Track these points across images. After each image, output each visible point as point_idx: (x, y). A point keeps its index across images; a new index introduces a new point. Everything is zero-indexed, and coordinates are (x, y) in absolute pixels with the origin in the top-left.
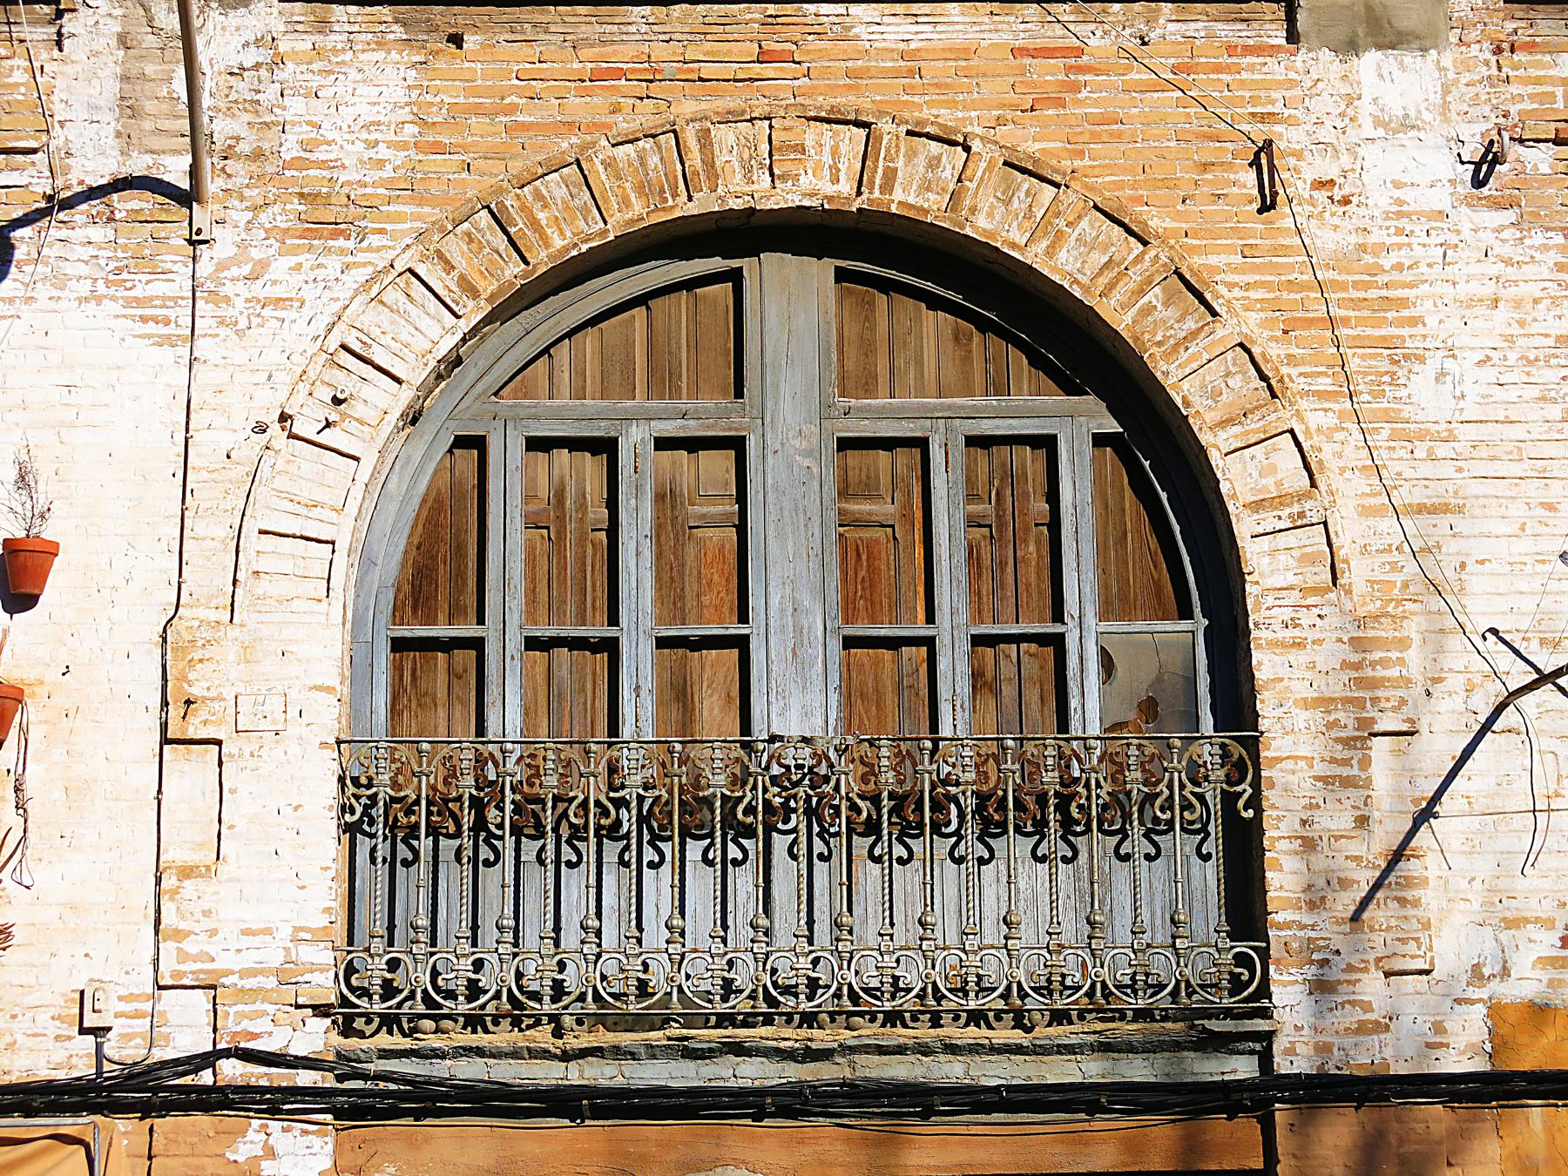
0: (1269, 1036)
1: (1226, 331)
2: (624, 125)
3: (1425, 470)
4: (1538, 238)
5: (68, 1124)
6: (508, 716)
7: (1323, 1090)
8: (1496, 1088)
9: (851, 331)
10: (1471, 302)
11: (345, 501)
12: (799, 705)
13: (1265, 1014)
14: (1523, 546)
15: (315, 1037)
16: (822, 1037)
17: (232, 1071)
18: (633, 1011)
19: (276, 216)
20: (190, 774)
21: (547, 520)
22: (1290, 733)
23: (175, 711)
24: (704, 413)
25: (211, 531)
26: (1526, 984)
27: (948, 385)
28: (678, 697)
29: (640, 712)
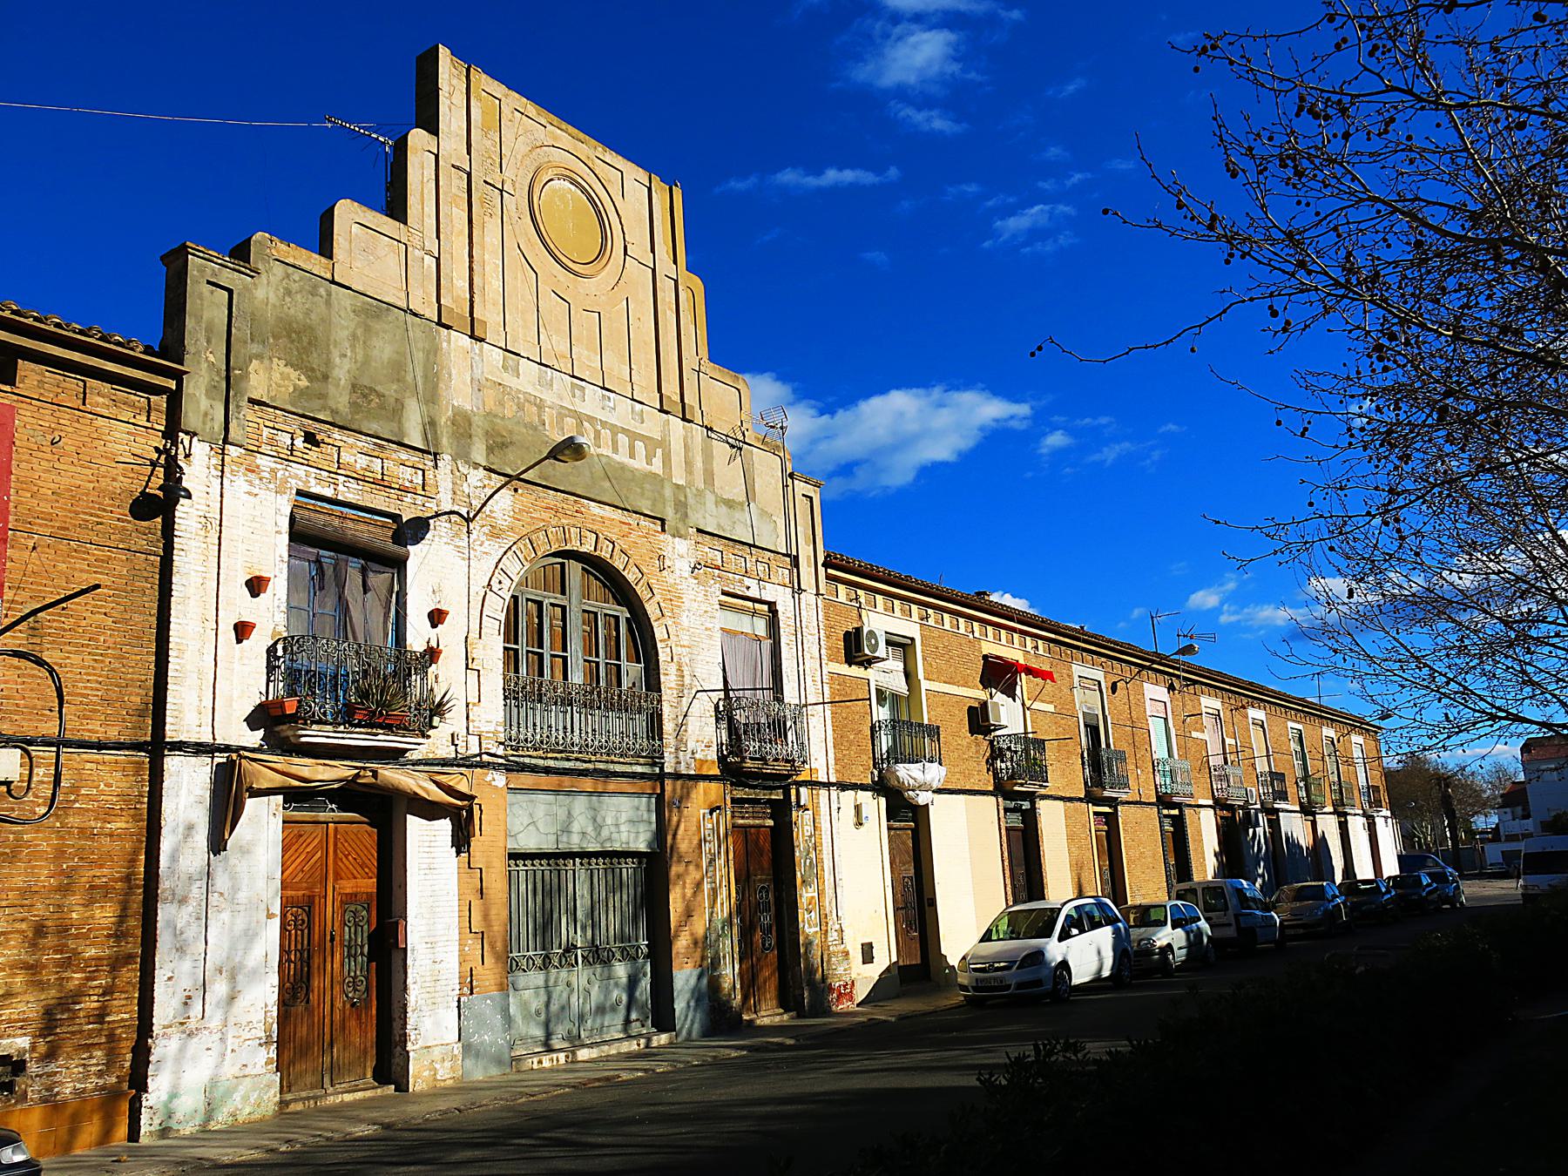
5: (463, 770)
11: (497, 608)
12: (577, 678)
17: (485, 758)
25: (475, 613)
29: (547, 671)
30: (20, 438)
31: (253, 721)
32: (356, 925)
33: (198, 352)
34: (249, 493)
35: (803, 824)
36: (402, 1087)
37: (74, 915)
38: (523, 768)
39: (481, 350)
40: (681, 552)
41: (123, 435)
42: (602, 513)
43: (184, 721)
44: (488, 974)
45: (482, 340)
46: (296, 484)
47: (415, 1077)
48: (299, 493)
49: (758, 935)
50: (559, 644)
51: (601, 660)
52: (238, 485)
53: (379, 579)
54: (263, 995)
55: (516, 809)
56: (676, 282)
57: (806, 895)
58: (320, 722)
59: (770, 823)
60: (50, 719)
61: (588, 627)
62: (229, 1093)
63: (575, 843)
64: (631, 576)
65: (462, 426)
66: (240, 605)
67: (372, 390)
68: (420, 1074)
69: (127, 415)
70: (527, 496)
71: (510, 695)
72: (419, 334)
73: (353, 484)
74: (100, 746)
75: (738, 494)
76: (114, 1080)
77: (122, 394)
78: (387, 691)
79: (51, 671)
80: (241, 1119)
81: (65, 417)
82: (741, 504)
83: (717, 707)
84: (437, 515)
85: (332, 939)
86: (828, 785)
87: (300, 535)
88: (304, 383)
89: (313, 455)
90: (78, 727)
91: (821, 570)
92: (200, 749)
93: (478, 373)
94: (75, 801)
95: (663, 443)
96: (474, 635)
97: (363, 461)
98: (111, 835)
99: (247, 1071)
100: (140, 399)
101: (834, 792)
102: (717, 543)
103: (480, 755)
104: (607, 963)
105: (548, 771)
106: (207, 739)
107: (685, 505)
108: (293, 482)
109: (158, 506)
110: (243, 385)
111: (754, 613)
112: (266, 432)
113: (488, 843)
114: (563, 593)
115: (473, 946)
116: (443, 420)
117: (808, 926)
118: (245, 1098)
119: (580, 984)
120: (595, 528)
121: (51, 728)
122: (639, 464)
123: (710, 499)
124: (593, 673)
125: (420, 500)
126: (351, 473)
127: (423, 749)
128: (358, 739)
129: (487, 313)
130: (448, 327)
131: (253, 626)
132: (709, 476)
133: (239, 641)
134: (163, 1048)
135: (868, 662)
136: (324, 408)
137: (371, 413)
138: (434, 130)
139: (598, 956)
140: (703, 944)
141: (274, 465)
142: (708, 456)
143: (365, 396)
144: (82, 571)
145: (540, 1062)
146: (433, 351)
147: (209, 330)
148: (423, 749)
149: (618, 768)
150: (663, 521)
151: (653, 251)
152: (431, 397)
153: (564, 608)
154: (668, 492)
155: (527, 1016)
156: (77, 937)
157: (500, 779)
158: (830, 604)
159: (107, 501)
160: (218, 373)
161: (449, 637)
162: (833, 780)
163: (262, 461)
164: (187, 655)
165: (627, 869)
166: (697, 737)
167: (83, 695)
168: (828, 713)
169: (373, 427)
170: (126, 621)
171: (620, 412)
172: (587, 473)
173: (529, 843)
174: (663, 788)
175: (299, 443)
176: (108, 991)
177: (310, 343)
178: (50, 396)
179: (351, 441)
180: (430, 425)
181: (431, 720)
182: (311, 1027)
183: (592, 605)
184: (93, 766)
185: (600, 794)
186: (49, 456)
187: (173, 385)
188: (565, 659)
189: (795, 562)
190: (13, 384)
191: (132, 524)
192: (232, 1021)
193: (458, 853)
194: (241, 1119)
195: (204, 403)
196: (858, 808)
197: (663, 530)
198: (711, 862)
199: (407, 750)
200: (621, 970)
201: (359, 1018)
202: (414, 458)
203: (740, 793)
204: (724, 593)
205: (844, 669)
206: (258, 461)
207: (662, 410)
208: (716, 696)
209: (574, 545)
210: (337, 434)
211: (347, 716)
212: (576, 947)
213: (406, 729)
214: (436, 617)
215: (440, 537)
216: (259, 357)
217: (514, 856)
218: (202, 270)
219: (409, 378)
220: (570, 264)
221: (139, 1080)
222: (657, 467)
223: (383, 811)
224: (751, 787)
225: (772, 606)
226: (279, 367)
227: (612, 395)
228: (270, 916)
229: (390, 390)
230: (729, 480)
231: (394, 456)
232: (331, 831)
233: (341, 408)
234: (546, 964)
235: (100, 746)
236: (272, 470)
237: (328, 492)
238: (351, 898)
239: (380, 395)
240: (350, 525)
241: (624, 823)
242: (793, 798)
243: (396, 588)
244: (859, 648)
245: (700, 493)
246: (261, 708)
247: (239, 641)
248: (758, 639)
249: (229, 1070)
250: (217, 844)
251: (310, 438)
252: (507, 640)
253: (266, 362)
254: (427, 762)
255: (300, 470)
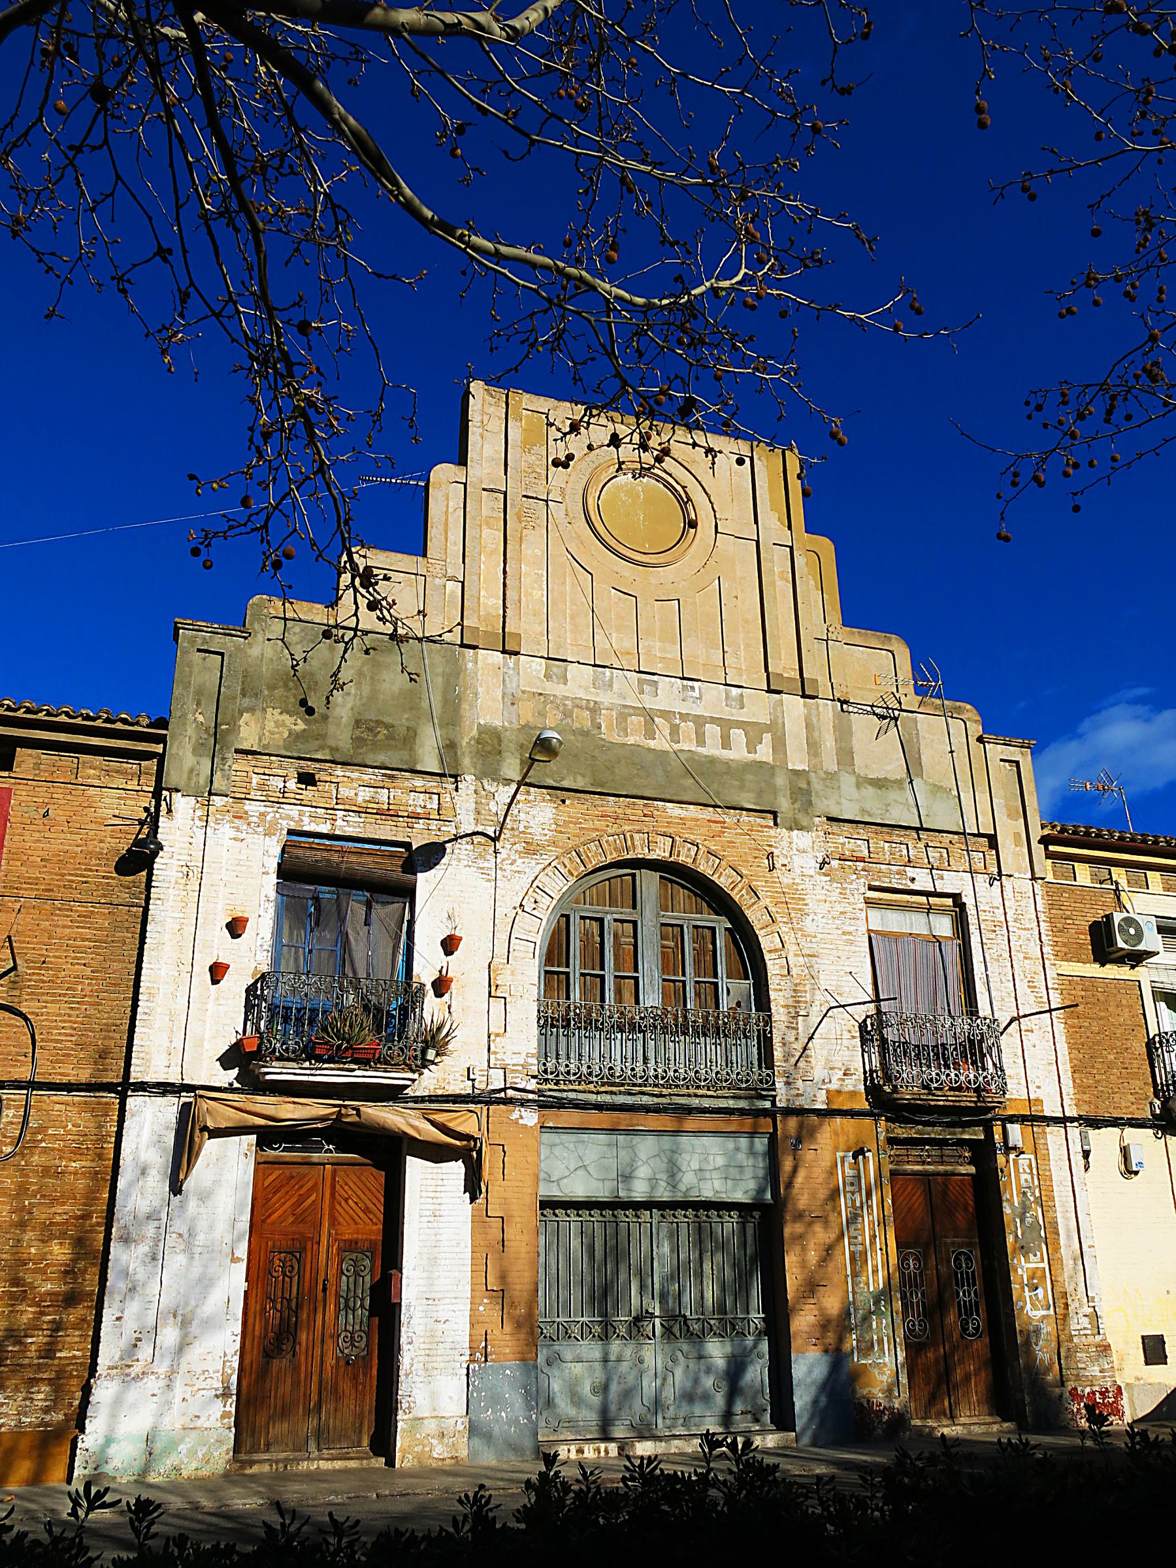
0: (775, 1097)
1: (762, 903)
2: (610, 831)
3: (810, 945)
4: (835, 885)
5: (472, 1106)
6: (576, 994)
7: (788, 1112)
8: (830, 1113)
9: (816, 734)
10: (819, 901)
11: (535, 931)
12: (651, 999)
13: (774, 1090)
14: (832, 967)
15: (532, 1085)
16: (665, 1092)
17: (510, 1093)
18: (609, 1080)
19: (518, 847)
20: (497, 1006)
21: (586, 937)
22: (779, 1013)
23: (493, 988)
24: (627, 913)
25: (502, 937)
26: (834, 1086)
27: (694, 917)
28: (619, 991)
29: (610, 996)
30: (14, 814)
31: (226, 1061)
32: (356, 1274)
33: (184, 715)
34: (235, 839)
35: (1017, 1175)
36: (390, 1462)
37: (33, 1250)
38: (560, 1104)
39: (517, 664)
40: (800, 849)
41: (112, 799)
42: (683, 813)
43: (150, 1064)
44: (505, 1341)
45: (517, 653)
46: (286, 825)
47: (403, 1451)
48: (291, 832)
49: (952, 1317)
50: (630, 960)
51: (687, 978)
52: (224, 832)
53: (385, 912)
54: (220, 1347)
55: (557, 1151)
56: (791, 548)
57: (1023, 1267)
58: (281, 1059)
59: (972, 1169)
60: (23, 1064)
61: (665, 947)
62: (172, 1445)
63: (639, 1191)
64: (723, 881)
65: (490, 745)
66: (221, 947)
67: (379, 723)
68: (409, 1446)
69: (120, 782)
70: (574, 807)
71: (547, 1023)
72: (438, 659)
73: (353, 818)
74: (69, 1087)
75: (895, 767)
76: (61, 1417)
77: (114, 763)
78: (395, 1024)
79: (26, 1019)
80: (185, 1473)
81: (59, 792)
82: (899, 782)
83: (862, 1027)
84: (456, 838)
85: (324, 1290)
86: (1063, 1121)
87: (289, 872)
88: (301, 726)
89: (309, 793)
90: (48, 1071)
91: (1039, 850)
92: (165, 1089)
93: (511, 686)
94: (41, 1141)
95: (776, 730)
96: (500, 960)
97: (364, 794)
98: (75, 1174)
99: (199, 1423)
100: (132, 766)
101: (1074, 1131)
102: (863, 832)
103: (504, 1090)
104: (696, 1339)
105: (599, 1107)
106: (175, 1078)
107: (808, 792)
108: (284, 823)
109: (139, 859)
110: (231, 738)
111: (929, 910)
112: (255, 779)
113: (511, 1188)
114: (634, 907)
115: (489, 1311)
116: (466, 740)
117: (1032, 1308)
118: (192, 1453)
119: (652, 1363)
120: (671, 831)
121: (23, 1073)
122: (738, 752)
123: (847, 782)
124: (674, 992)
125: (434, 825)
126: (351, 808)
127: (427, 1082)
128: (330, 1075)
129: (526, 626)
130: (475, 647)
131: (227, 967)
132: (846, 756)
133: (215, 981)
134: (103, 1392)
135: (1137, 958)
136: (321, 748)
137: (380, 744)
138: (462, 461)
139: (679, 1328)
140: (836, 1329)
141: (263, 809)
142: (843, 733)
143: (370, 730)
144: (64, 927)
145: (580, 1451)
146: (455, 674)
147: (199, 693)
148: (427, 1082)
149: (706, 1103)
150: (775, 814)
151: (756, 522)
152: (452, 715)
153: (635, 923)
154: (781, 781)
155: (576, 1399)
156: (35, 1271)
157: (530, 1118)
158: (1055, 895)
159: (94, 862)
160: (207, 730)
161: (466, 968)
162: (1071, 1112)
163: (249, 806)
164: (159, 999)
165: (730, 1224)
166: (830, 1062)
167: (57, 1041)
168: (1059, 1028)
169: (381, 758)
170: (105, 970)
171: (710, 700)
172: (659, 772)
173: (578, 1189)
174: (774, 1125)
175: (292, 784)
176: (57, 1326)
177: (309, 688)
178: (45, 776)
179: (355, 775)
180: (450, 748)
181: (424, 1052)
182: (296, 1384)
183: (671, 917)
184: (63, 1107)
185: (677, 1133)
186: (41, 827)
187: (159, 748)
188: (636, 979)
189: (993, 841)
190: (10, 769)
191: (116, 879)
192: (183, 1368)
193: (473, 1199)
194: (185, 1473)
195: (189, 760)
196: (1125, 1152)
197: (776, 824)
198: (853, 1219)
199: (407, 1086)
200: (717, 1351)
201: (355, 1378)
202: (432, 784)
203: (901, 1132)
204: (871, 888)
205: (1094, 970)
206: (246, 808)
207: (769, 691)
208: (860, 1012)
209: (641, 852)
210: (339, 771)
211: (309, 1054)
212: (652, 1316)
213: (387, 1063)
214: (450, 945)
215: (457, 859)
216: (251, 710)
217: (547, 1205)
218: (192, 641)
219: (425, 704)
220: (638, 557)
221: (80, 1421)
222: (764, 752)
223: (387, 1153)
224: (925, 1124)
225: (956, 897)
226: (273, 716)
227: (696, 684)
228: (235, 1260)
229: (402, 720)
230: (878, 752)
231: (407, 784)
232: (328, 1174)
233: (341, 744)
234: (606, 1333)
235: (69, 1087)
236: (263, 814)
237: (324, 828)
238: (350, 1246)
239: (388, 726)
240: (353, 858)
241: (716, 1167)
242: (998, 1137)
243: (407, 917)
244: (1112, 941)
245: (831, 777)
246: (236, 1047)
247: (215, 981)
248: (937, 940)
249: (173, 1421)
250: (176, 1187)
251: (307, 779)
252: (665, 969)
253: (258, 713)
254: (422, 1099)
255: (294, 811)
